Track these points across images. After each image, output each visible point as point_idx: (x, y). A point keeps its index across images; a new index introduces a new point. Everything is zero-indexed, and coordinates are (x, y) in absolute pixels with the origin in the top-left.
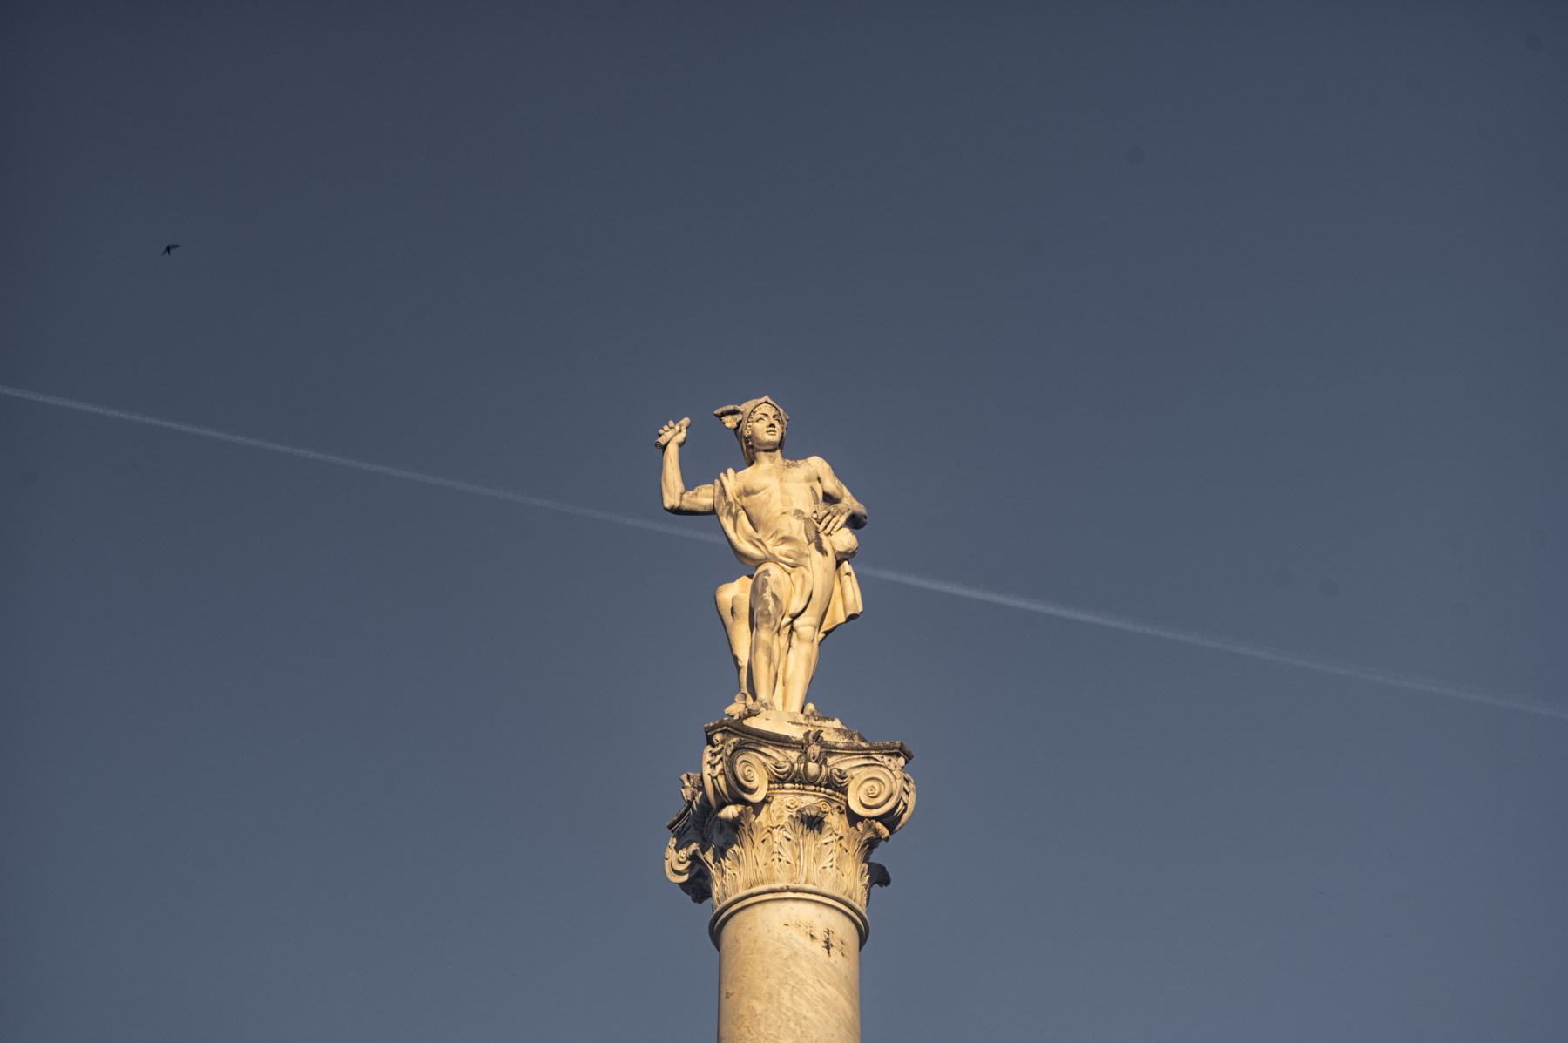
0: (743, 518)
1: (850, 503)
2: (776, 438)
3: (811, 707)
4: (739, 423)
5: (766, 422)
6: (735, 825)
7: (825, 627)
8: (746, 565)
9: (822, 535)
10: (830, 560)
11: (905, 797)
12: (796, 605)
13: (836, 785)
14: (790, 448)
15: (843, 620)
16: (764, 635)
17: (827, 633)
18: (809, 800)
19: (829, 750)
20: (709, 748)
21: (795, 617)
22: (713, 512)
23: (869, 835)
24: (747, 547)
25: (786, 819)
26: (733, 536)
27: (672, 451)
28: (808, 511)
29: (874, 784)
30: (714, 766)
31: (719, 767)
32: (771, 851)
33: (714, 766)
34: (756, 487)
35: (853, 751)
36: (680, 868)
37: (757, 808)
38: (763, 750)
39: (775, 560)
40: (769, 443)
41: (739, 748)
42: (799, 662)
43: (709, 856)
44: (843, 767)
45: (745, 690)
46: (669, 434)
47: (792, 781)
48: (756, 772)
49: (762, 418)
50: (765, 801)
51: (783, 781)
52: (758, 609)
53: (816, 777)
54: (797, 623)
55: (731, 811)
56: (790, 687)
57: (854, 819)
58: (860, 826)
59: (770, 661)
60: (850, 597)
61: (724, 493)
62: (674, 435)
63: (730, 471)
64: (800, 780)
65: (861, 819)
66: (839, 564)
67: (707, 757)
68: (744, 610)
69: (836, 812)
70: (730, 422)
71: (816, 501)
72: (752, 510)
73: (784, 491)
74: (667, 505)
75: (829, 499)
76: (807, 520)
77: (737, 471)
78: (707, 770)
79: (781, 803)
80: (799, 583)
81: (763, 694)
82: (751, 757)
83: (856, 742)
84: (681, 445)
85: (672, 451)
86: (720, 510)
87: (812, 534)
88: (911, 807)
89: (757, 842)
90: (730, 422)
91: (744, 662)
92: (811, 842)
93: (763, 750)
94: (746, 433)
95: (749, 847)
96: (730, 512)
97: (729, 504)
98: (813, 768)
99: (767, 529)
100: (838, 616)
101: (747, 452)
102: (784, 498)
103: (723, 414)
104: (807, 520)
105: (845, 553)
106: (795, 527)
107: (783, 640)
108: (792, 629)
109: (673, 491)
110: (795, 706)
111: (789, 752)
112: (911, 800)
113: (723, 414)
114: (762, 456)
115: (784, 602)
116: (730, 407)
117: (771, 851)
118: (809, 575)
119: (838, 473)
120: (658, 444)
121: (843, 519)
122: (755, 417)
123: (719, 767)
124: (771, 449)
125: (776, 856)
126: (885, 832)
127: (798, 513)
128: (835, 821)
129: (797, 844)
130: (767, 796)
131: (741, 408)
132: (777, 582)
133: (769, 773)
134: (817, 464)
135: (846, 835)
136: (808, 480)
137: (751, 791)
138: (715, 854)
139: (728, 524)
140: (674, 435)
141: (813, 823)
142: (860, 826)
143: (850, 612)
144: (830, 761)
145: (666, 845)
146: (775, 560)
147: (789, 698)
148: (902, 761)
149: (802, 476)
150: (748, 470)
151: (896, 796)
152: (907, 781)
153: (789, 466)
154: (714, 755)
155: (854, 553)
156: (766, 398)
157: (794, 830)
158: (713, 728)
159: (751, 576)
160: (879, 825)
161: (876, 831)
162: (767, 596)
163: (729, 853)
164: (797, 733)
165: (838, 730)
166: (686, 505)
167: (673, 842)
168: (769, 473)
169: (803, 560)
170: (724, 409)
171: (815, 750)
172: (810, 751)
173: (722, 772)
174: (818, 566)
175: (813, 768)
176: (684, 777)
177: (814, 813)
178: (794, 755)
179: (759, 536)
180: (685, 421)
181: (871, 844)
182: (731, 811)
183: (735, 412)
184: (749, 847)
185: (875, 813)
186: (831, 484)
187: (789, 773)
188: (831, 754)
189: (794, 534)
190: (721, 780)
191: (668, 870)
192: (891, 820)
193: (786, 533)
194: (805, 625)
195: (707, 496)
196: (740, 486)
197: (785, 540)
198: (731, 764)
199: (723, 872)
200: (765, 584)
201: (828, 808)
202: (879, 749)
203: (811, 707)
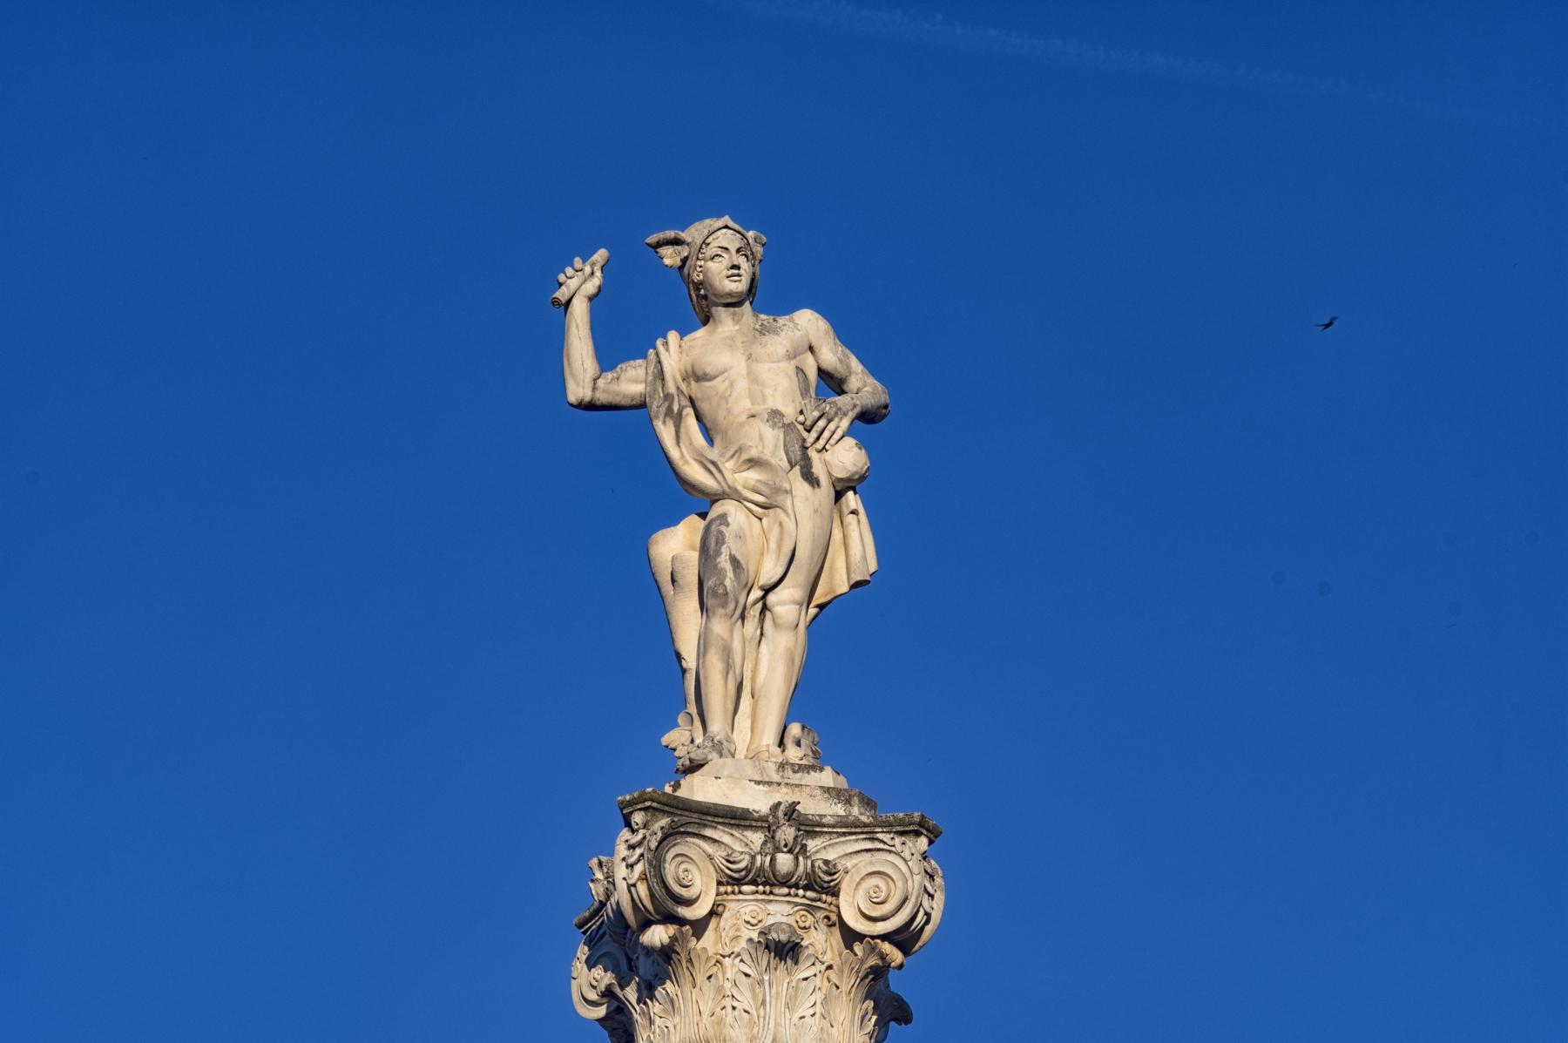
0: (691, 422)
1: (864, 387)
2: (741, 286)
3: (795, 729)
4: (685, 261)
5: (726, 261)
6: (666, 953)
7: (819, 598)
8: (700, 501)
9: (812, 453)
10: (826, 491)
11: (926, 903)
12: (770, 570)
13: (822, 885)
14: (768, 296)
15: (843, 588)
16: (719, 627)
17: (821, 607)
18: (780, 912)
19: (809, 827)
20: (625, 834)
22: (643, 405)
23: (873, 961)
24: (695, 472)
25: (743, 944)
26: (674, 453)
27: (580, 308)
28: (789, 412)
29: (884, 881)
30: (631, 866)
31: (639, 868)
32: (720, 993)
33: (631, 866)
34: (709, 370)
35: (848, 827)
36: (593, 996)
37: (699, 927)
38: (708, 832)
39: (740, 498)
40: (730, 294)
41: (669, 835)
42: (774, 660)
43: (631, 994)
44: (831, 855)
45: (692, 708)
46: (573, 284)
47: (754, 882)
48: (696, 872)
49: (721, 251)
50: (713, 913)
51: (739, 882)
52: (710, 583)
53: (791, 875)
54: (772, 598)
55: (658, 935)
56: (763, 702)
57: (851, 937)
58: (858, 948)
59: (728, 667)
60: (856, 551)
61: (660, 375)
62: (580, 283)
63: (673, 336)
64: (765, 880)
66: (839, 496)
67: (622, 850)
68: (690, 576)
69: (823, 927)
70: (670, 256)
71: (805, 392)
72: (704, 407)
73: (753, 378)
74: (572, 399)
75: (831, 382)
76: (788, 428)
77: (683, 335)
78: (621, 872)
79: (737, 915)
80: (774, 535)
81: (717, 726)
82: (691, 847)
83: (855, 811)
84: (591, 299)
85: (580, 308)
86: (656, 405)
88: (936, 916)
89: (700, 978)
90: (670, 256)
91: (690, 662)
92: (782, 978)
93: (708, 832)
94: (697, 277)
95: (688, 987)
96: (669, 412)
97: (668, 397)
98: (784, 861)
99: (727, 442)
100: (837, 581)
101: (701, 306)
102: (754, 389)
103: (659, 245)
104: (788, 428)
105: (849, 480)
106: (768, 441)
107: (751, 626)
108: (765, 608)
109: (582, 373)
110: (769, 737)
111: (749, 834)
112: (937, 907)
113: (659, 245)
114: (721, 313)
115: (752, 569)
116: (671, 234)
117: (720, 993)
118: (789, 524)
119: (845, 334)
120: (556, 302)
121: (845, 423)
123: (639, 868)
124: (734, 302)
125: (728, 1002)
126: (896, 956)
127: (775, 415)
128: (820, 942)
129: (761, 983)
130: (716, 905)
131: (683, 235)
132: (740, 537)
133: (718, 870)
134: (808, 323)
135: (836, 963)
136: (792, 355)
137: (689, 903)
138: (639, 991)
139: (666, 432)
140: (580, 283)
141: (785, 950)
142: (858, 948)
143: (857, 578)
144: (812, 844)
145: (572, 955)
146: (740, 498)
147: (759, 723)
148: (923, 843)
149: (781, 351)
150: (701, 333)
151: (912, 900)
152: (932, 877)
153: (764, 330)
154: (632, 847)
155: (862, 478)
156: (726, 220)
158: (631, 803)
159: (703, 515)
160: (886, 947)
161: (882, 956)
162: (724, 562)
163: (659, 992)
164: (758, 801)
165: (827, 790)
166: (602, 397)
167: (583, 951)
168: (730, 344)
169: (780, 498)
170: (661, 236)
171: (787, 833)
172: (779, 835)
173: (643, 877)
174: (805, 502)
175: (784, 861)
176: (594, 862)
177: (783, 937)
178: (756, 838)
179: (713, 454)
180: (601, 255)
181: (878, 973)
182: (658, 935)
183: (677, 242)
184: (688, 987)
186: (831, 355)
187: (748, 870)
188: (813, 834)
189: (767, 455)
190: (642, 889)
191: (576, 996)
192: (904, 938)
193: (754, 453)
194: (785, 601)
195: (636, 381)
196: (686, 362)
197: (753, 463)
198: (657, 864)
199: (651, 1022)
200: (721, 540)
201: (810, 920)
202: (888, 826)
203: (795, 729)
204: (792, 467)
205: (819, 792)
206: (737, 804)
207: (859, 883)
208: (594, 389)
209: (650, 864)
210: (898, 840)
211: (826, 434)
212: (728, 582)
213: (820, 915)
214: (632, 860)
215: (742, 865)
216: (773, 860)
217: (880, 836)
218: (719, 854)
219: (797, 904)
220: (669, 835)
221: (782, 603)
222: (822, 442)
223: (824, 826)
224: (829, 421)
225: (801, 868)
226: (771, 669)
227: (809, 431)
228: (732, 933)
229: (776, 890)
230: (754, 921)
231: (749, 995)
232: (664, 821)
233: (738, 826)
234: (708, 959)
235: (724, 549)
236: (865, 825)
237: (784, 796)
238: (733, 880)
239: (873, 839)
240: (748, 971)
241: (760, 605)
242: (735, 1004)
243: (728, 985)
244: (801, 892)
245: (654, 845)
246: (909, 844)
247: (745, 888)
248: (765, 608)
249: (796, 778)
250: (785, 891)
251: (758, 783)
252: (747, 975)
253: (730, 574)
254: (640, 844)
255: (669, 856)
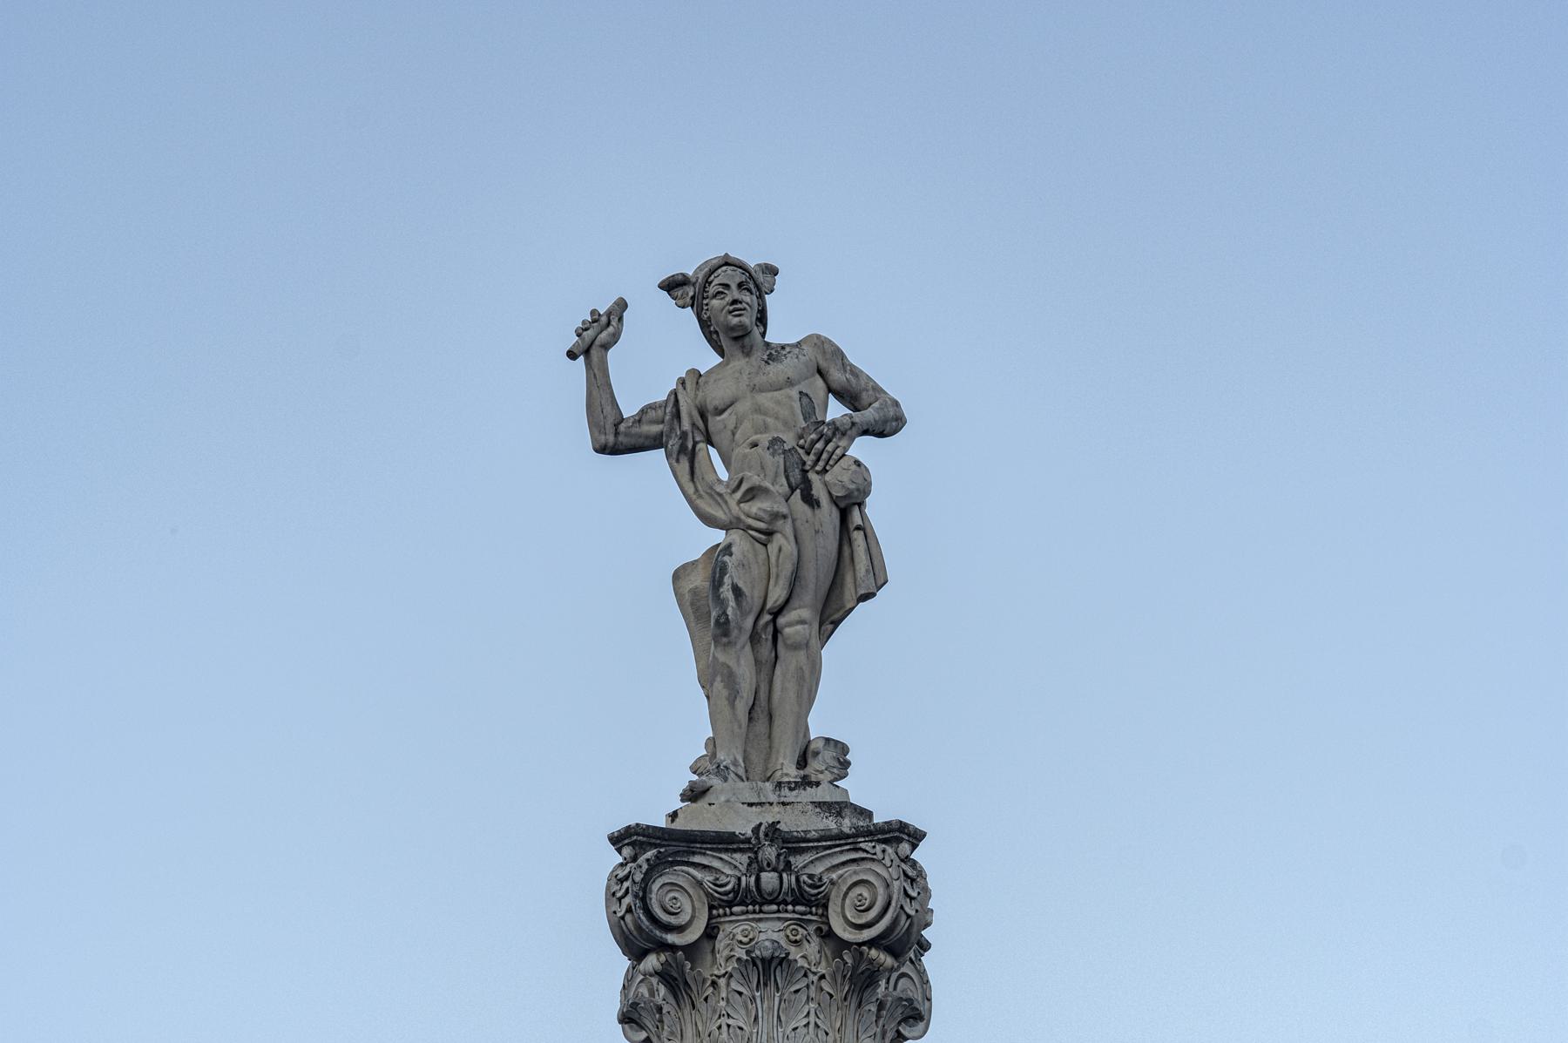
9: (812, 476)
12: (777, 595)
18: (770, 933)
19: (792, 844)
21: (777, 613)
28: (790, 440)
31: (627, 900)
38: (697, 859)
44: (818, 869)
51: (731, 904)
54: (781, 621)
56: (777, 722)
65: (847, 945)
87: (796, 476)
93: (697, 859)
98: (769, 879)
111: (737, 856)
122: (712, 290)
125: (724, 1020)
128: (809, 953)
137: (680, 929)
141: (767, 968)
144: (798, 861)
157: (746, 979)
164: (742, 825)
171: (769, 852)
175: (769, 879)
178: (742, 859)
185: (867, 934)
187: (735, 891)
204: (793, 490)
205: (810, 807)
206: (730, 829)
207: (846, 894)
208: (617, 434)
209: (636, 896)
210: (879, 848)
211: (825, 456)
212: (730, 612)
213: (812, 928)
214: (619, 895)
215: (729, 887)
216: (758, 880)
217: (862, 845)
218: (707, 878)
219: (787, 920)
220: (654, 868)
221: (790, 625)
222: (821, 463)
223: (809, 841)
224: (827, 443)
225: (785, 885)
226: (783, 689)
227: (808, 453)
228: (726, 953)
229: (765, 908)
230: (745, 940)
231: (743, 1012)
232: (650, 854)
233: (727, 850)
234: (704, 981)
235: (727, 580)
236: (848, 836)
237: (768, 817)
238: (723, 903)
239: (856, 850)
240: (741, 989)
241: (770, 629)
242: (730, 1022)
243: (723, 1004)
244: (790, 907)
245: (638, 877)
246: (890, 850)
247: (736, 909)
248: (776, 633)
249: (791, 796)
250: (775, 907)
251: (751, 805)
252: (740, 994)
253: (732, 603)
254: (626, 878)
255: (655, 887)
